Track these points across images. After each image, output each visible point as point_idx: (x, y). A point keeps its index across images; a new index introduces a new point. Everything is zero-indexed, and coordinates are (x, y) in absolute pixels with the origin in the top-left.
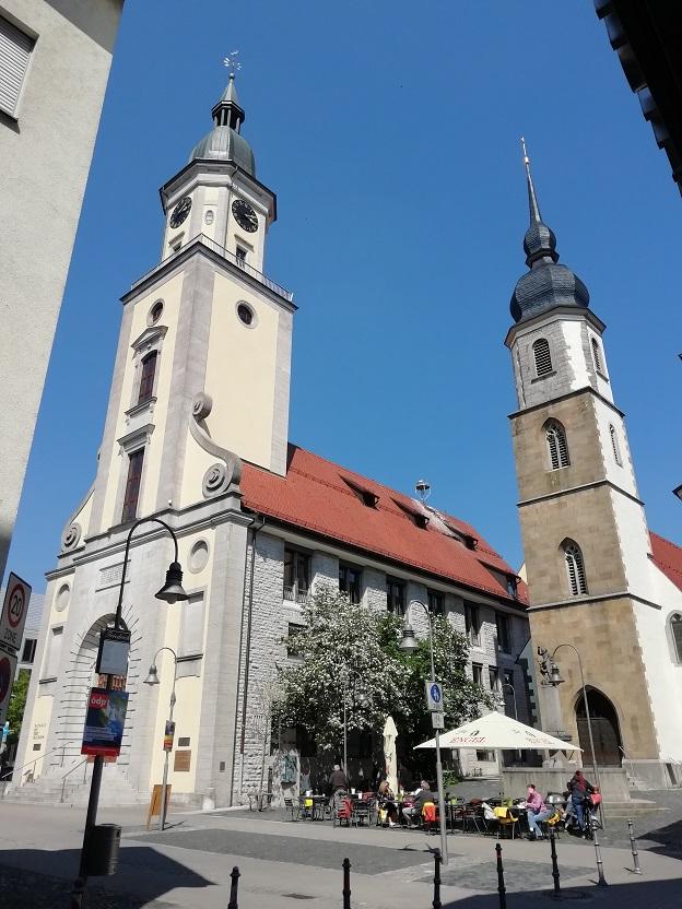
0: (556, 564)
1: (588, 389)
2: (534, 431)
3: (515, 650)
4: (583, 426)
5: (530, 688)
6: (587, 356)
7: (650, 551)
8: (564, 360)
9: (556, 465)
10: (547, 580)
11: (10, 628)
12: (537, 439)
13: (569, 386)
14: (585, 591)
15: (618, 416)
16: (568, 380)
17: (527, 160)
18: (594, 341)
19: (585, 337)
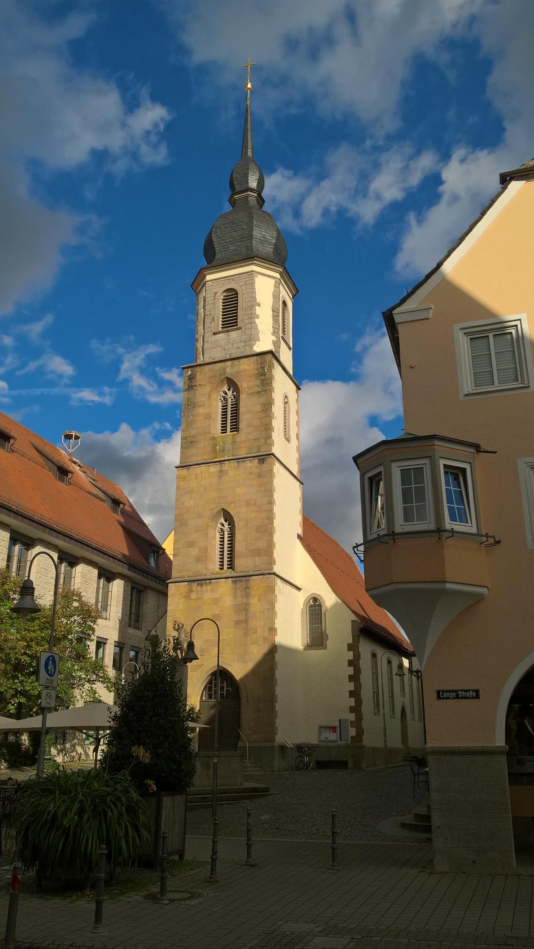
0: (207, 534)
1: (271, 352)
2: (207, 389)
3: (147, 625)
4: (259, 392)
5: (353, 699)
6: (275, 317)
7: (300, 532)
8: (252, 316)
9: (224, 431)
10: (195, 551)
11: (49, 677)
12: (209, 398)
13: (251, 346)
14: (231, 566)
15: (294, 387)
16: (253, 338)
17: (249, 86)
18: (284, 303)
19: (276, 295)
